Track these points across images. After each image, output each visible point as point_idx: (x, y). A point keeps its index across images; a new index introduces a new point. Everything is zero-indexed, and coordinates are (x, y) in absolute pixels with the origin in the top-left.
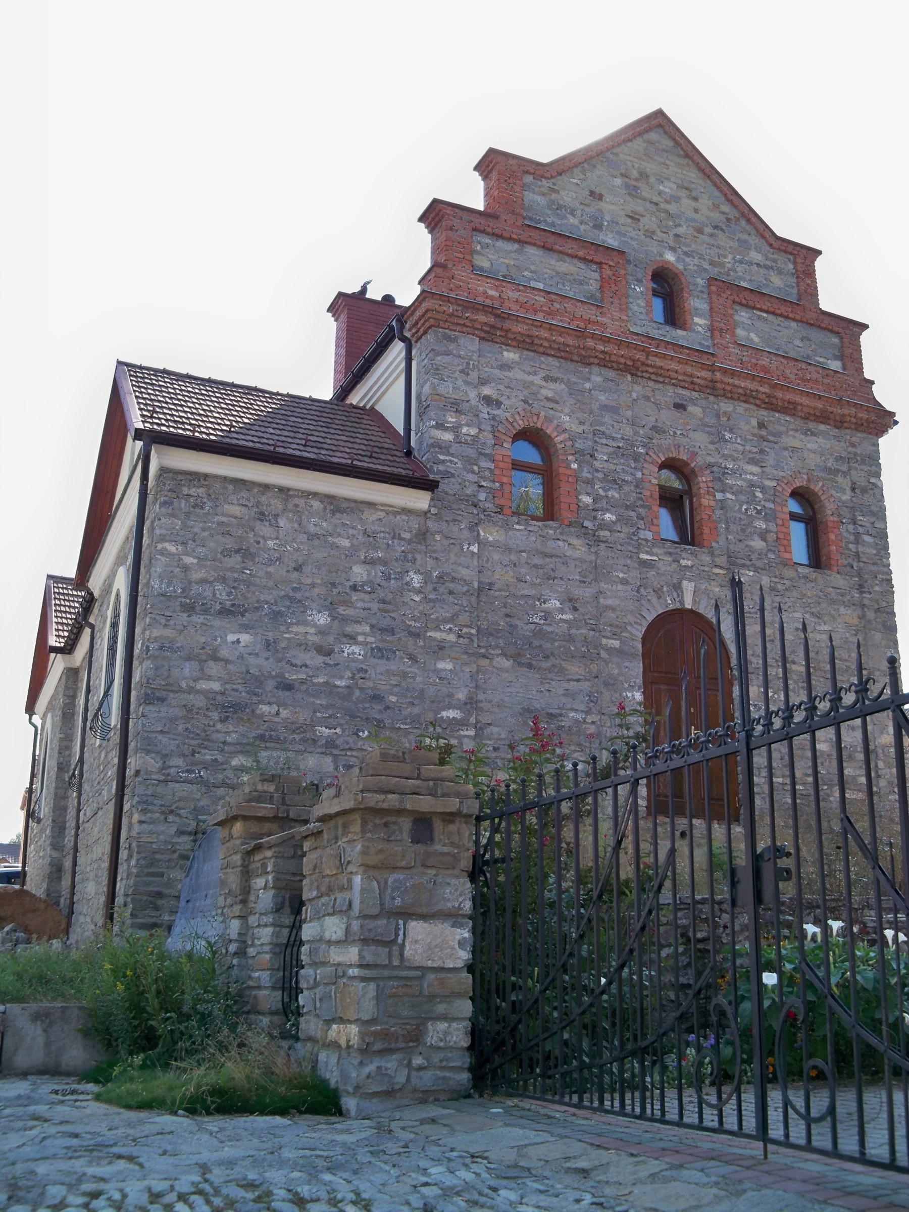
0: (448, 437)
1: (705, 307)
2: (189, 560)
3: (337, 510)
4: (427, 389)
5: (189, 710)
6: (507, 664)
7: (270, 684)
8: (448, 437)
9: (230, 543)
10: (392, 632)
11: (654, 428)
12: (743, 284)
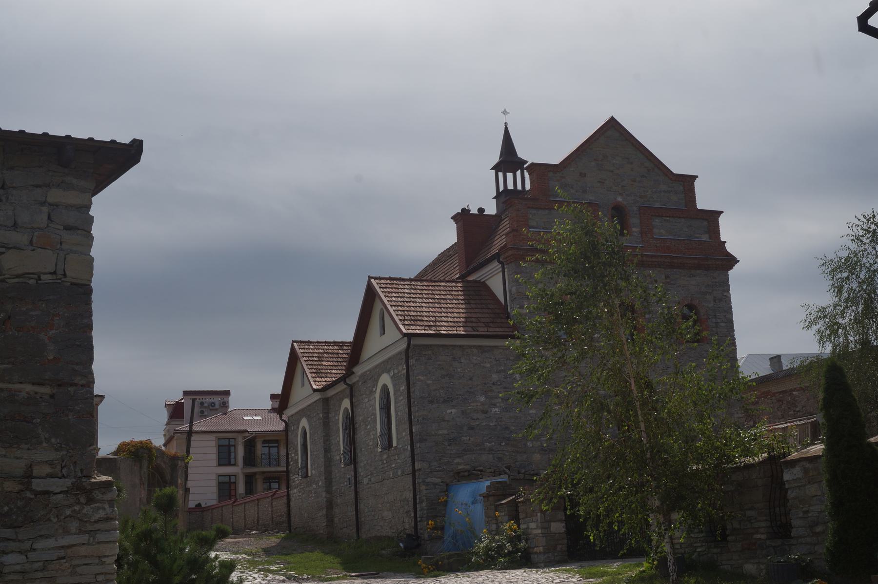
2: (429, 382)
4: (514, 289)
12: (657, 205)
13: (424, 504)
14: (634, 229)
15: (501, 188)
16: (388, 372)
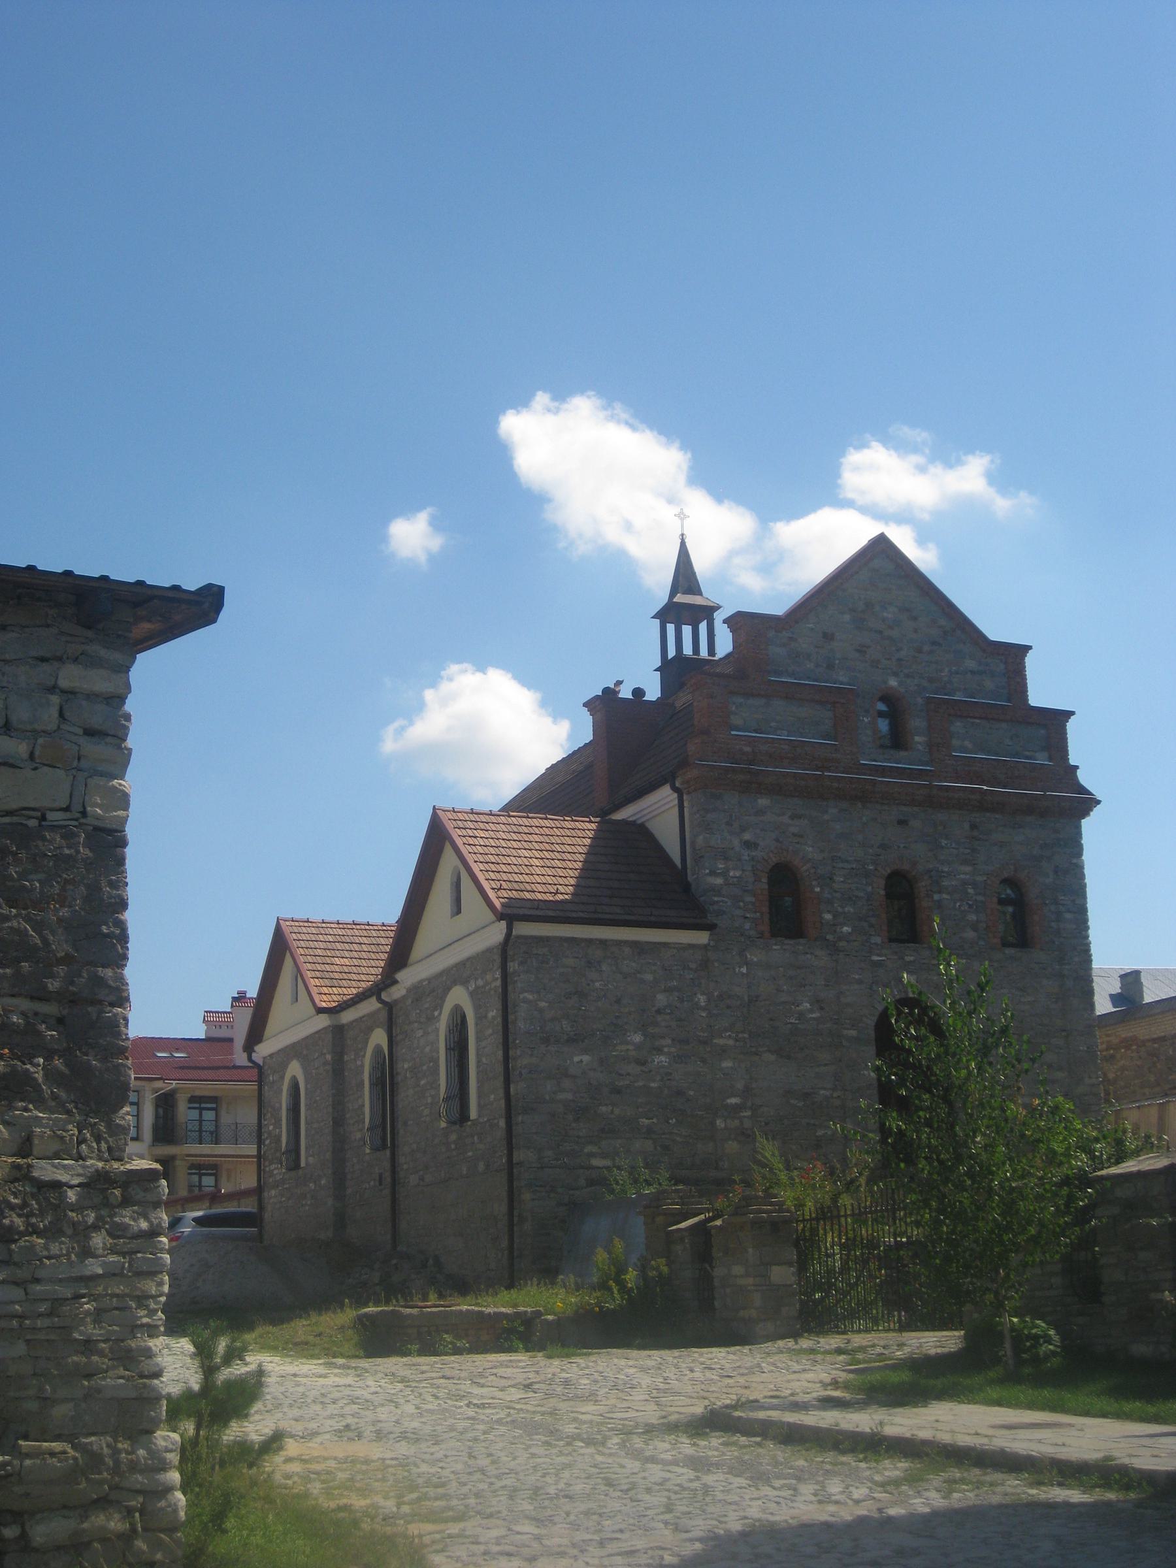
0: (719, 881)
2: (543, 1004)
6: (773, 1057)
8: (719, 881)
11: (883, 846)
14: (917, 739)
15: (671, 653)
16: (465, 983)
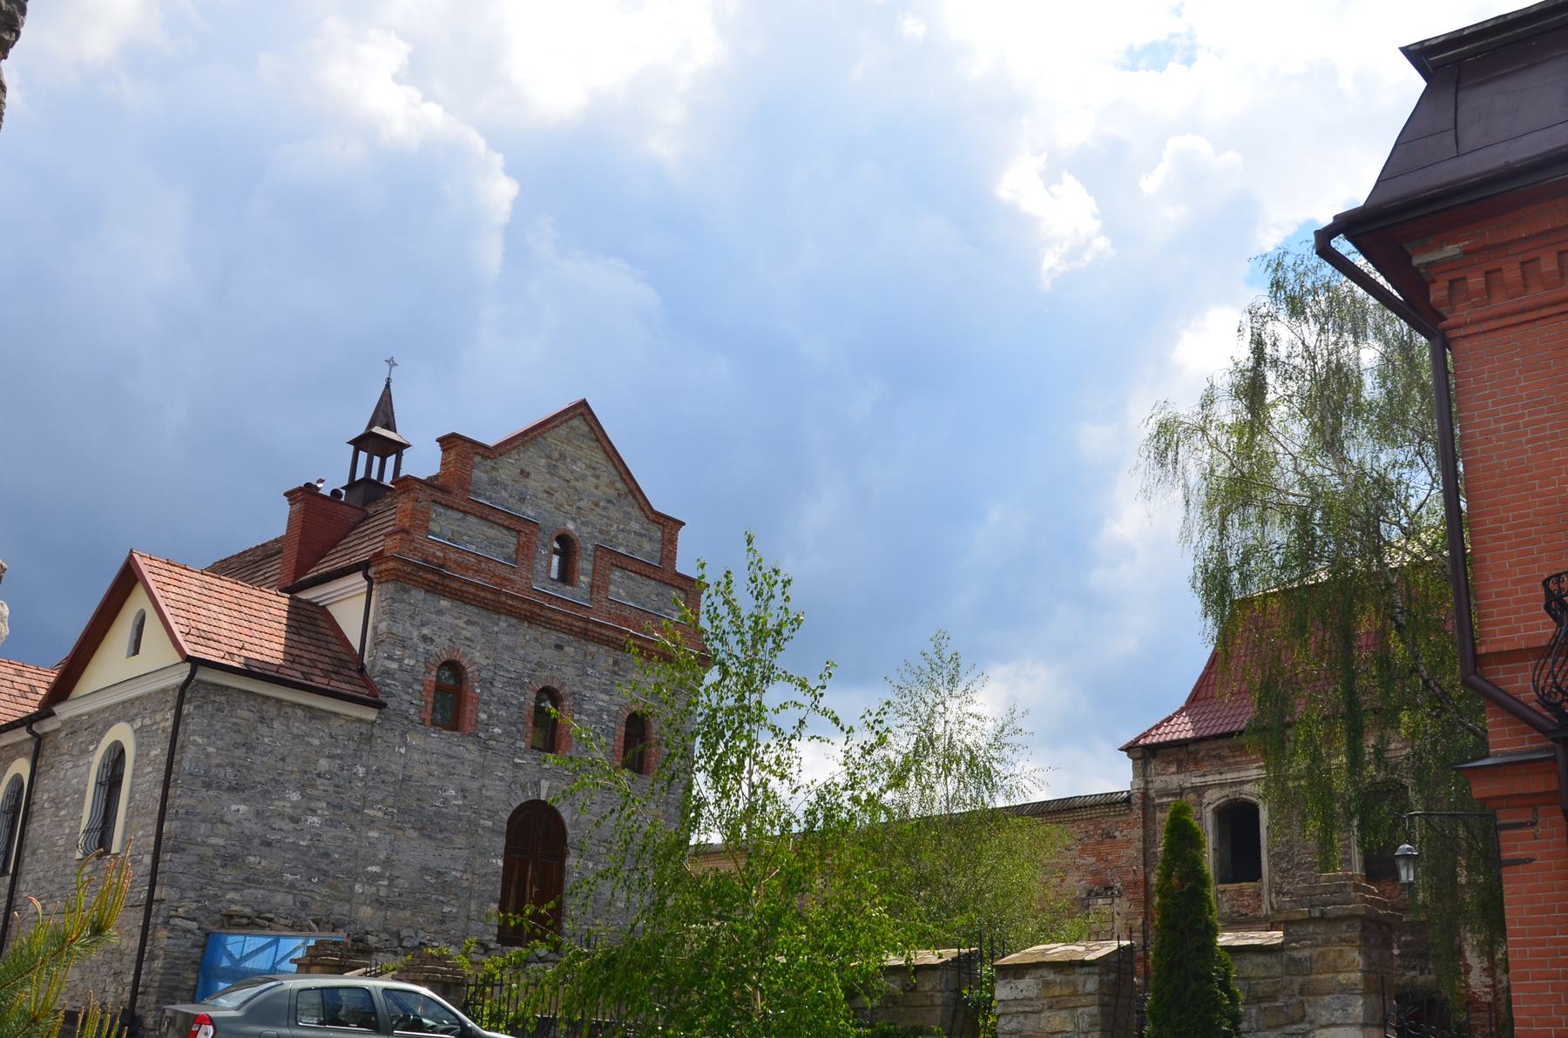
0: (394, 666)
1: (590, 567)
2: (211, 750)
3: (314, 717)
4: (383, 626)
5: (202, 859)
6: (414, 834)
7: (256, 842)
8: (394, 666)
9: (239, 738)
10: (341, 808)
11: (539, 664)
12: (621, 550)
13: (158, 964)
15: (360, 475)
16: (131, 720)
